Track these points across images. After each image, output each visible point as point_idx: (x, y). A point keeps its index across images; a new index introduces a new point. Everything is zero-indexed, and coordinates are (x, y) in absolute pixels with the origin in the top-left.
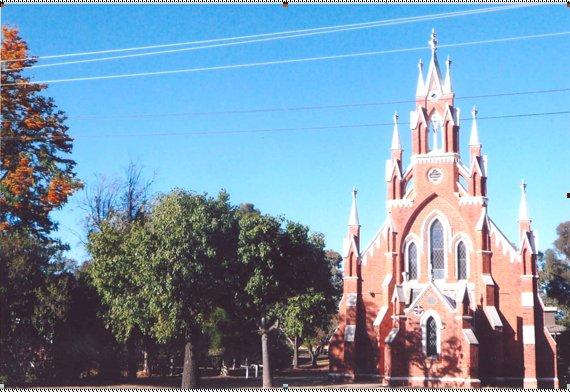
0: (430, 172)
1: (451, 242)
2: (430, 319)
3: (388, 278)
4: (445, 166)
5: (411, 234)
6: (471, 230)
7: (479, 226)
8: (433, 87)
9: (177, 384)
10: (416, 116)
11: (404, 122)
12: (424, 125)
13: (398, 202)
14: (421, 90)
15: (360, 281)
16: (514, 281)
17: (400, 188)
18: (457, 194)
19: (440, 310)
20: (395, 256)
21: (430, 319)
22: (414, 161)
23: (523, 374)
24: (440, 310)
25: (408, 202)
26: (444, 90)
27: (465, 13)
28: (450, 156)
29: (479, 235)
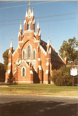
0: (28, 34)
1: (32, 50)
2: (24, 68)
3: (18, 59)
4: (31, 33)
5: (23, 49)
6: (36, 49)
7: (38, 47)
8: (30, 14)
9: (72, 86)
10: (25, 21)
11: (22, 24)
12: (21, 36)
13: (20, 42)
14: (27, 15)
15: (12, 60)
16: (45, 60)
17: (21, 38)
18: (33, 40)
19: (25, 66)
20: (19, 54)
21: (24, 68)
22: (25, 32)
23: (5, 79)
24: (25, 66)
25: (22, 42)
26: (32, 15)
27: (9, 57)
28: (32, 31)
29: (38, 49)
